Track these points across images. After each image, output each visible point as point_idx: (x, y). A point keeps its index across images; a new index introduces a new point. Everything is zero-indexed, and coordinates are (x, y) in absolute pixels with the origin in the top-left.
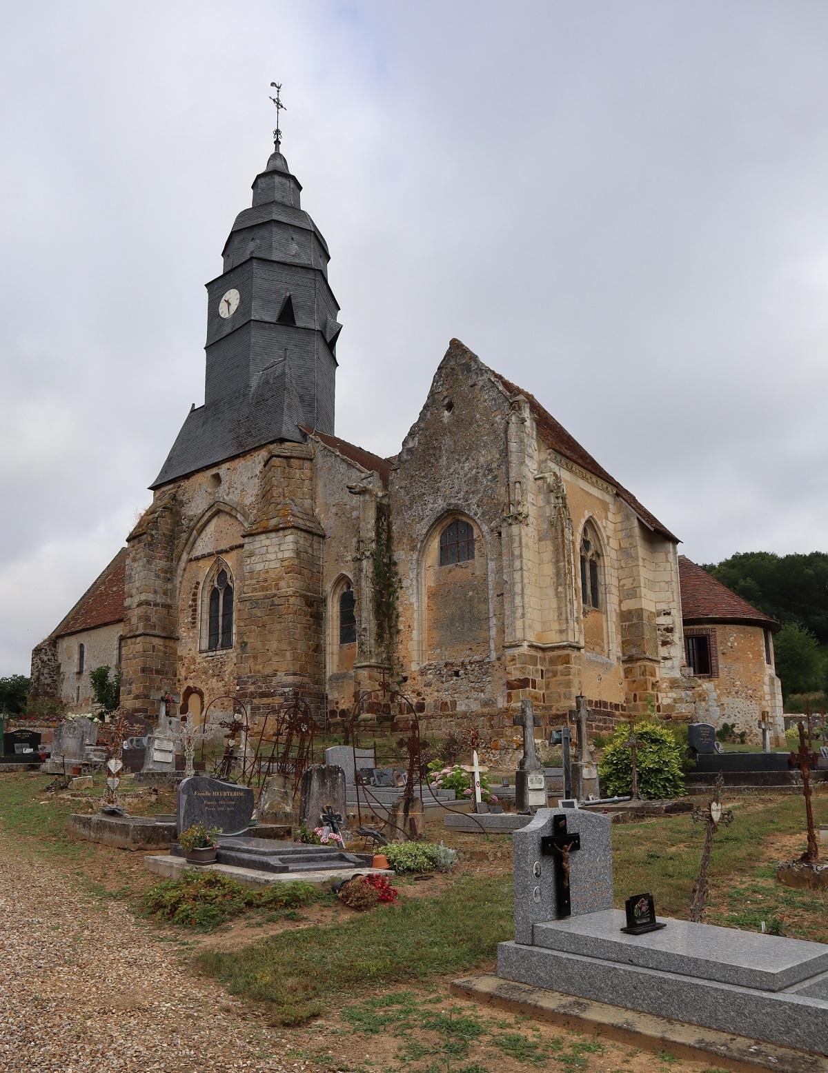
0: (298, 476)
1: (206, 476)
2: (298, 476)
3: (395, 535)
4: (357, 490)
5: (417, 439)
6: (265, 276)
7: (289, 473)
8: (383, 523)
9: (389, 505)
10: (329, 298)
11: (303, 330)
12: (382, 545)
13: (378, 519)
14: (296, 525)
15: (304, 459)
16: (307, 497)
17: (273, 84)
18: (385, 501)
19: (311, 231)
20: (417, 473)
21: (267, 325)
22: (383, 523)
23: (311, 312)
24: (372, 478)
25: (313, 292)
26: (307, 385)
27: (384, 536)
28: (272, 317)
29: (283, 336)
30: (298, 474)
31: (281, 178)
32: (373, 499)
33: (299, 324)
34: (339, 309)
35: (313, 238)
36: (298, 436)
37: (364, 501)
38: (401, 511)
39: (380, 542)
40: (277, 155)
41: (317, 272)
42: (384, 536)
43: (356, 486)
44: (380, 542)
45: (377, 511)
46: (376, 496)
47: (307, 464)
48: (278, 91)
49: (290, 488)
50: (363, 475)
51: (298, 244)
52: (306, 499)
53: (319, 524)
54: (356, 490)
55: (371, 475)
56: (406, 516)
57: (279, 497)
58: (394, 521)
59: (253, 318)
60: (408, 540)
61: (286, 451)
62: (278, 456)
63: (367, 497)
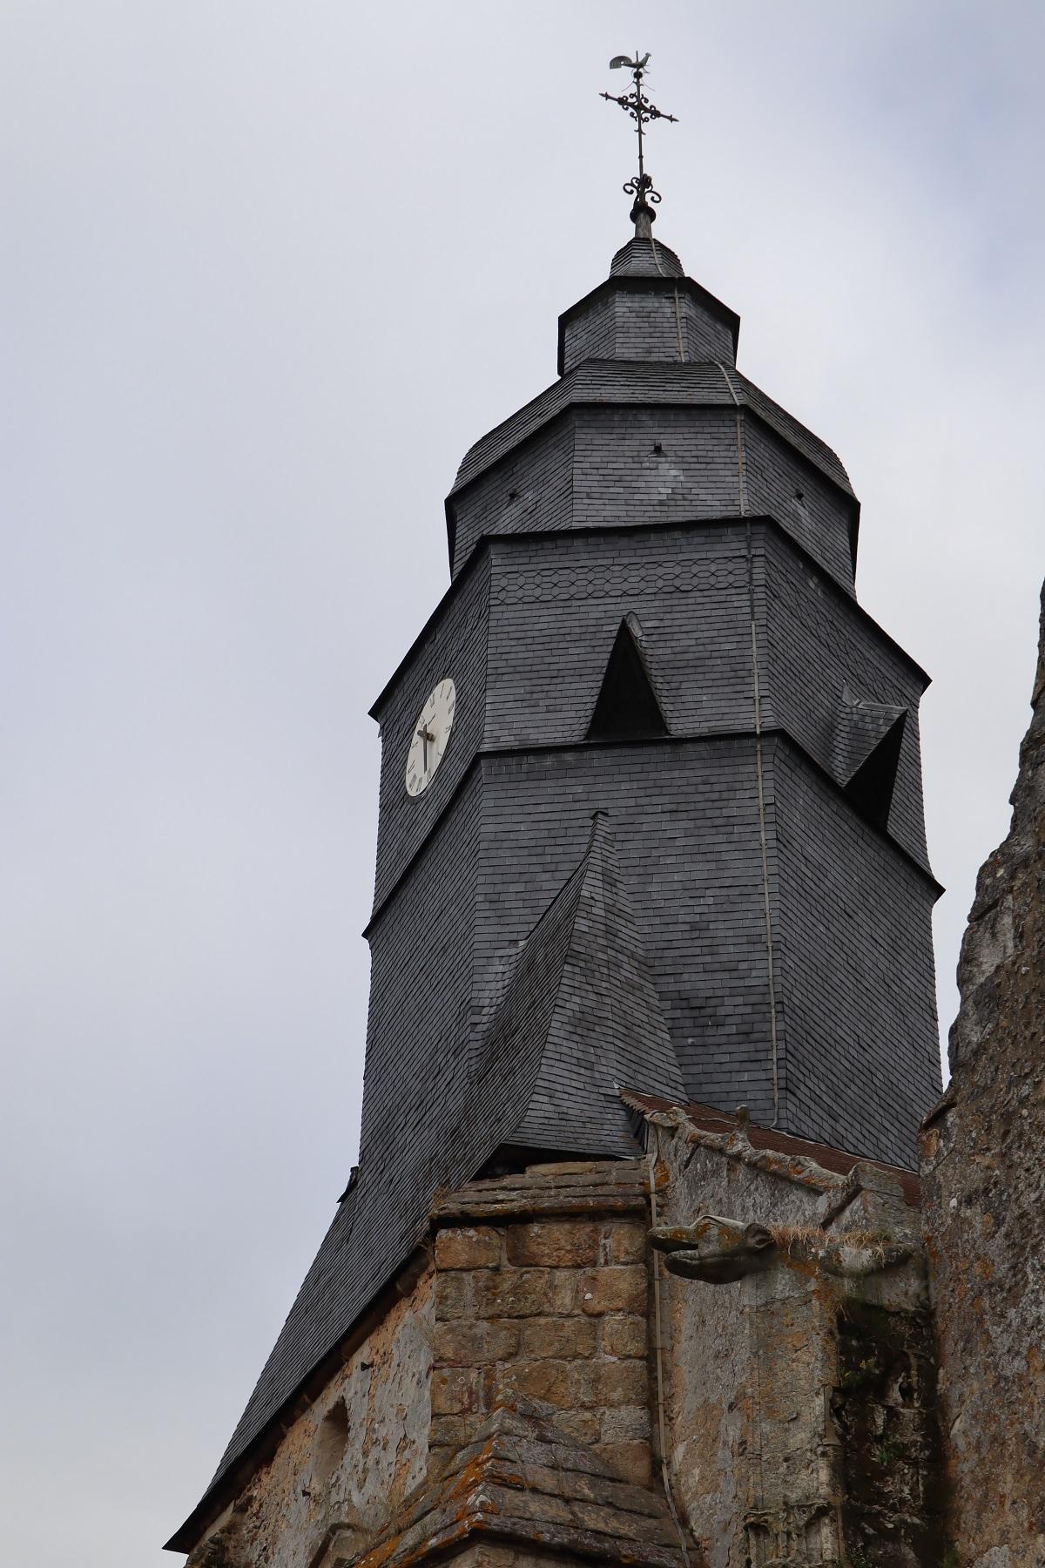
0: (565, 1299)
1: (312, 1427)
2: (565, 1299)
3: (964, 1468)
4: (709, 1249)
5: (1007, 920)
6: (538, 592)
7: (518, 1291)
8: (892, 1413)
9: (925, 1317)
10: (873, 654)
11: (701, 747)
12: (893, 1536)
13: (851, 1398)
14: (495, 1522)
15: (597, 1215)
16: (616, 1396)
17: (618, 62)
18: (899, 1293)
19: (734, 407)
20: (1025, 1090)
21: (549, 761)
22: (892, 1413)
23: (738, 675)
24: (856, 1204)
25: (742, 601)
26: (728, 953)
27: (902, 1486)
28: (568, 718)
29: (618, 784)
30: (565, 1291)
31: (637, 297)
32: (812, 1286)
33: (679, 726)
34: (923, 680)
35: (740, 430)
36: (613, 1132)
37: (767, 1309)
38: (980, 1322)
39: (873, 1519)
40: (642, 241)
41: (749, 529)
42: (902, 1486)
43: (702, 1231)
44: (873, 1519)
45: (844, 1350)
46: (831, 1266)
47: (619, 1239)
48: (638, 75)
49: (522, 1361)
50: (822, 1205)
51: (680, 461)
52: (612, 1405)
53: (684, 1521)
54: (706, 1250)
55: (853, 1192)
56: (1003, 1342)
57: (465, 1411)
58: (954, 1395)
59: (486, 747)
60: (1019, 1475)
61: (514, 1195)
62: (463, 1221)
63: (783, 1283)
